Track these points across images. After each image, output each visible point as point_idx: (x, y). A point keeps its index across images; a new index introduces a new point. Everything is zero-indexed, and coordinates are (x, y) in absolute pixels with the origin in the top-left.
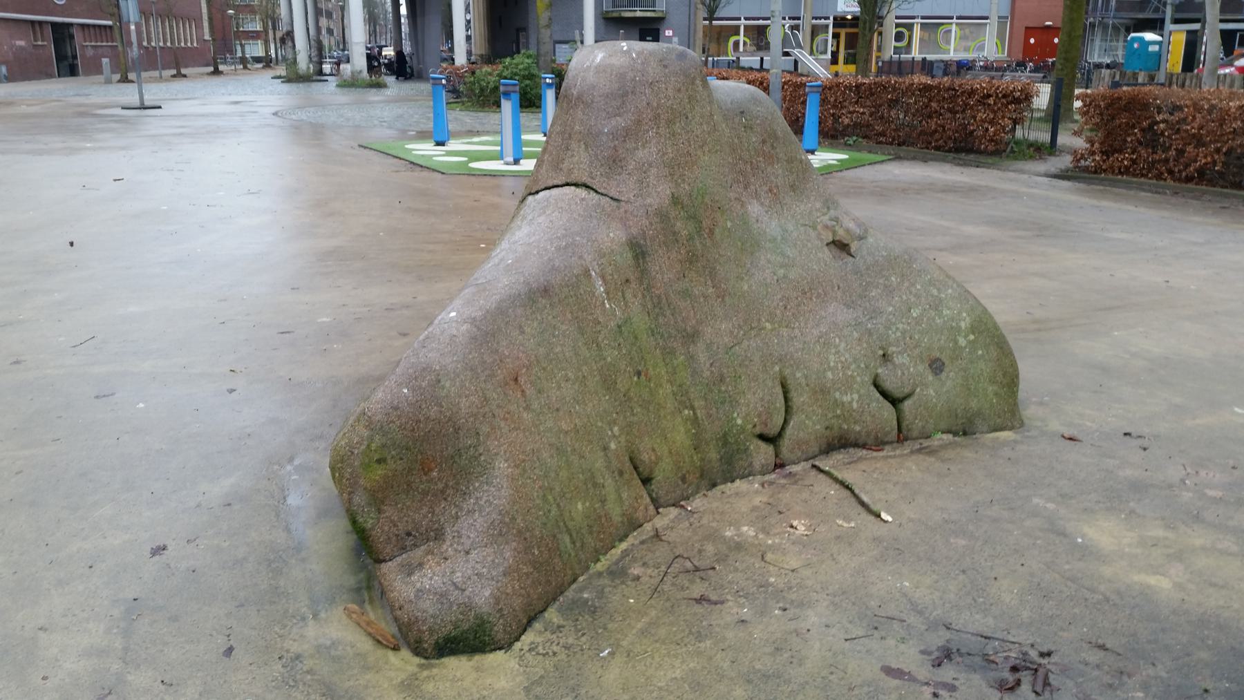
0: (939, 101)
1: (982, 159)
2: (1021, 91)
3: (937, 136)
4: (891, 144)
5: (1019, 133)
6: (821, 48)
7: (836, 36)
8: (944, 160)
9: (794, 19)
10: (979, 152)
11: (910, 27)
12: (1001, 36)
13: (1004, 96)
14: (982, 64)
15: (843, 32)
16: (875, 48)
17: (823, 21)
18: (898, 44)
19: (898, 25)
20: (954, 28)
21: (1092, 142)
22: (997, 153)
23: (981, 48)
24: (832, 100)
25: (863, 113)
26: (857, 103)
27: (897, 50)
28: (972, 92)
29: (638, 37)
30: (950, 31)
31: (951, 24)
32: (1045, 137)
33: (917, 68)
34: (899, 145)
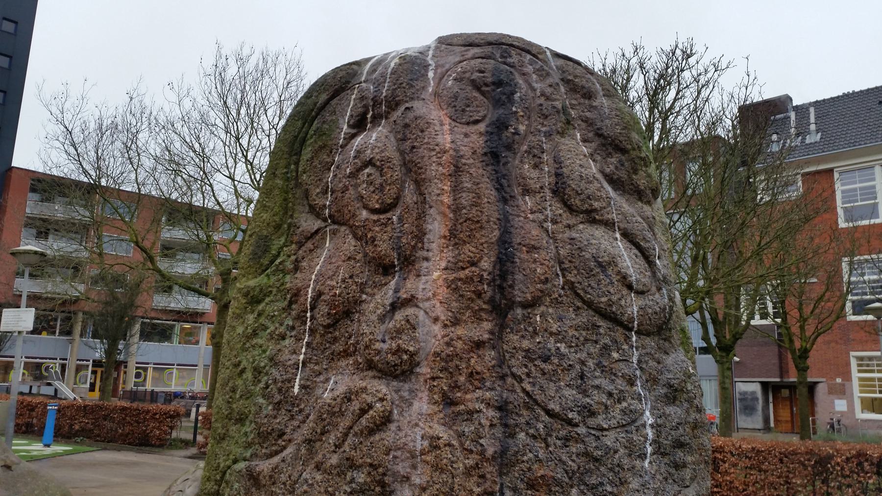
0: (130, 417)
1: (154, 449)
2: (174, 411)
3: (130, 436)
4: (103, 441)
6: (83, 380)
7: (94, 372)
8: (131, 450)
9: (64, 359)
10: (153, 446)
11: (145, 370)
12: (205, 377)
13: (165, 414)
14: (190, 394)
16: (121, 381)
17: (85, 362)
18: (137, 380)
19: (137, 368)
22: (161, 446)
23: (192, 384)
24: (69, 414)
25: (88, 423)
26: (84, 416)
29: (14, 175)
31: (173, 368)
32: (190, 437)
34: (108, 442)
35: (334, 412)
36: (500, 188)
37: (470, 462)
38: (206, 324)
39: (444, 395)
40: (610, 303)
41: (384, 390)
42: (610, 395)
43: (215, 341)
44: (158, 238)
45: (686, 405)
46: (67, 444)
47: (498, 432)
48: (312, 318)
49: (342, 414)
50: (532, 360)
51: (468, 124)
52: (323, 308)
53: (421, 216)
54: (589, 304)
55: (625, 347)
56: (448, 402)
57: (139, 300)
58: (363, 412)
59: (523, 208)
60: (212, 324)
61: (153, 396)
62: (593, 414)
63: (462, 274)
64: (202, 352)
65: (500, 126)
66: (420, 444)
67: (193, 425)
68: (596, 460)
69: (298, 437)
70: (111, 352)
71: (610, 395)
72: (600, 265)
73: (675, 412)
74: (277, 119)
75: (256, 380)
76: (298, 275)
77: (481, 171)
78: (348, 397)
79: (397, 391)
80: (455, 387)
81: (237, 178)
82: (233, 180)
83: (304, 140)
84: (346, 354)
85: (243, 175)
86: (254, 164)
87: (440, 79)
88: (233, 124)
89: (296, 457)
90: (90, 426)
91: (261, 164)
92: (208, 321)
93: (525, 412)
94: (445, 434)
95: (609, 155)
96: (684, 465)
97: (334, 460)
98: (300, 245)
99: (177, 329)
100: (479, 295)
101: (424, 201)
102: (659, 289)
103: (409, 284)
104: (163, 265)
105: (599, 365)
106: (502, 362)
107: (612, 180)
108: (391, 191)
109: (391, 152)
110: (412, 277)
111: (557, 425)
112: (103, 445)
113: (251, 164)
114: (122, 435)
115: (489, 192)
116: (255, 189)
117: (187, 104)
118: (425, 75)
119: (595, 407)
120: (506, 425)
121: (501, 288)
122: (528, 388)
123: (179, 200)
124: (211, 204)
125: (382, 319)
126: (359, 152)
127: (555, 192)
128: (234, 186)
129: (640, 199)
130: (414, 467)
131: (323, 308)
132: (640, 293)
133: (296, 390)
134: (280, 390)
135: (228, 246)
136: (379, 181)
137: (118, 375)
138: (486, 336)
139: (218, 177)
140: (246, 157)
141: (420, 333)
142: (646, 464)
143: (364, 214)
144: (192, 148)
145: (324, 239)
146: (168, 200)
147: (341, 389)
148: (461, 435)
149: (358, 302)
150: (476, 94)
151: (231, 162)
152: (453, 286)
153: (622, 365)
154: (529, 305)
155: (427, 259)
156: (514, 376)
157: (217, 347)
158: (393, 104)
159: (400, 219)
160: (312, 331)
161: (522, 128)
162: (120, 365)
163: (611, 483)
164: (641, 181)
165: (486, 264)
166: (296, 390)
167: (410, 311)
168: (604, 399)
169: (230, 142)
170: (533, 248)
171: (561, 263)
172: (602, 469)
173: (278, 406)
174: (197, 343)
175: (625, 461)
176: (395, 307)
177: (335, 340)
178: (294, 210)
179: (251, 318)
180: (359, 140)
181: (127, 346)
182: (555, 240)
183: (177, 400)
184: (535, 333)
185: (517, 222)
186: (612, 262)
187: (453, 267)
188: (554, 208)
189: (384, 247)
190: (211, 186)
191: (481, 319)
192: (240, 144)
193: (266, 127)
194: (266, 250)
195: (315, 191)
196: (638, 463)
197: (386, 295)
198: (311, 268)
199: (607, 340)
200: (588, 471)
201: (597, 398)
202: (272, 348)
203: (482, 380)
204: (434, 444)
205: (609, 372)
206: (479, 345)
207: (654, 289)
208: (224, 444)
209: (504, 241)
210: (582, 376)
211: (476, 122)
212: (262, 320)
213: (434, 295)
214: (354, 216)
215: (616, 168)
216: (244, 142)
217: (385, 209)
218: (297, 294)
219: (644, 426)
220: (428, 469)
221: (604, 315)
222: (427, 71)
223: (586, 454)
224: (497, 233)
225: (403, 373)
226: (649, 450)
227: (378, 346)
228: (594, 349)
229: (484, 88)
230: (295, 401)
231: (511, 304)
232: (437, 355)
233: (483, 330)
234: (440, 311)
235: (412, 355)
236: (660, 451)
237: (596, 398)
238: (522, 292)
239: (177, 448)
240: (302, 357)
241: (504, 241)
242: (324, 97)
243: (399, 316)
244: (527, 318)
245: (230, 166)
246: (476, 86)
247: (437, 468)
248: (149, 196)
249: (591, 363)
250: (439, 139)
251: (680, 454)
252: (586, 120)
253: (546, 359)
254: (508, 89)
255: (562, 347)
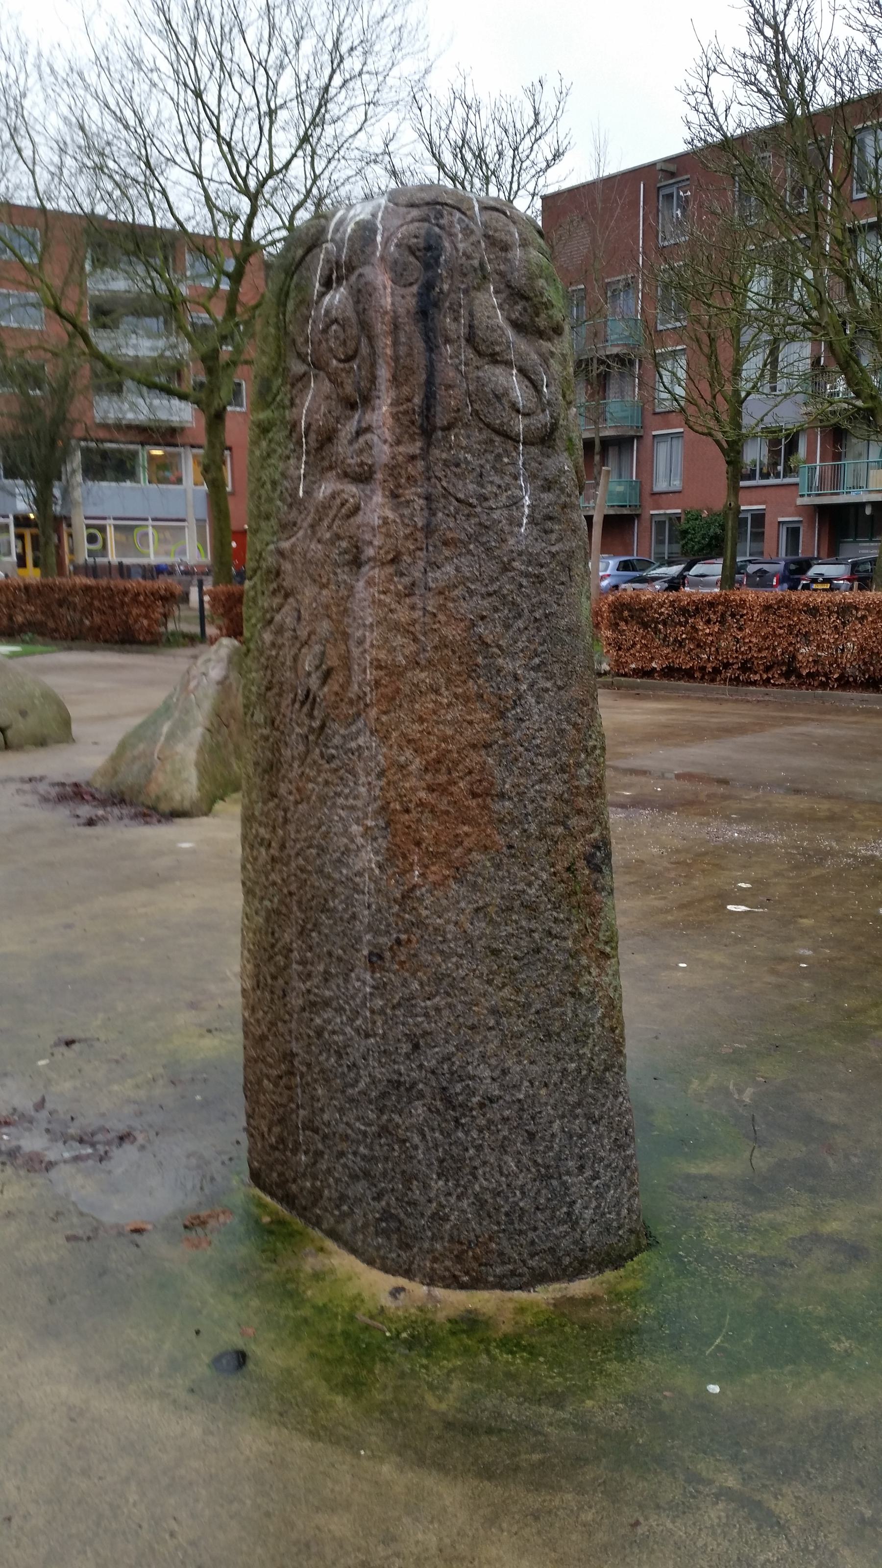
1: (143, 648)
5: (171, 626)
7: (20, 537)
8: (111, 650)
10: (143, 643)
11: (102, 529)
14: (182, 568)
15: (27, 533)
18: (93, 547)
19: (88, 527)
20: (151, 531)
21: (220, 629)
23: (183, 552)
27: (91, 553)
28: (125, 592)
30: (147, 534)
33: (115, 573)
34: (73, 639)
35: (325, 506)
36: (428, 340)
37: (408, 531)
38: (188, 449)
39: (392, 492)
40: (502, 424)
41: (354, 490)
42: (499, 487)
43: (209, 476)
44: (83, 291)
45: (558, 492)
46: (9, 643)
47: (426, 513)
48: (307, 443)
49: (330, 507)
50: (448, 467)
51: (405, 286)
52: (313, 436)
53: (373, 365)
54: (488, 426)
55: (514, 454)
56: (395, 496)
57: (75, 409)
58: (343, 505)
59: (444, 354)
60: (200, 447)
61: (123, 571)
62: (486, 499)
63: (401, 409)
64: (190, 496)
65: (428, 286)
66: (377, 522)
67: (198, 614)
68: (486, 527)
69: (305, 525)
70: (43, 501)
71: (499, 487)
72: (496, 396)
73: (548, 497)
74: (264, 48)
75: (274, 489)
76: (294, 410)
77: (413, 328)
78: (333, 496)
79: (363, 491)
80: (399, 486)
81: (206, 174)
82: (200, 177)
83: (287, 294)
84: (331, 468)
85: (215, 165)
86: (233, 144)
87: (386, 242)
88: (187, 64)
89: (305, 536)
90: (39, 617)
91: (246, 139)
92: (192, 441)
93: (442, 500)
94: (390, 515)
95: (516, 303)
96: (552, 531)
97: (328, 535)
98: (293, 385)
99: (142, 459)
100: (413, 422)
101: (374, 353)
102: (543, 411)
103: (367, 417)
104: (103, 342)
105: (493, 467)
106: (428, 468)
107: (516, 325)
108: (351, 345)
109: (350, 313)
110: (369, 412)
111: (463, 507)
112: (65, 644)
113: (229, 145)
114: (91, 628)
115: (419, 345)
116: (239, 192)
117: (101, 33)
118: (375, 240)
119: (488, 495)
120: (430, 509)
121: (427, 417)
122: (445, 484)
123: (112, 217)
124: (165, 221)
125: (351, 443)
126: (327, 312)
127: (468, 340)
128: (205, 190)
129: (541, 337)
130: (374, 536)
131: (313, 436)
132: (526, 415)
133: (301, 493)
134: (290, 495)
135: (207, 304)
136: (342, 337)
137: (60, 539)
138: (418, 452)
139: (174, 173)
140: (217, 131)
141: (375, 451)
142: (522, 530)
143: (334, 362)
144: (121, 120)
145: (307, 386)
146: (91, 218)
147: (329, 491)
148: (402, 516)
149: (335, 431)
150: (412, 259)
151: (192, 141)
152: (395, 417)
153: (510, 467)
154: (447, 428)
155: (379, 398)
156: (436, 477)
157: (216, 486)
158: (351, 268)
159: (359, 367)
160: (308, 453)
161: (446, 287)
162: (61, 522)
163: (495, 541)
164: (542, 322)
165: (417, 400)
166: (301, 493)
167: (368, 436)
168: (495, 489)
169: (186, 102)
170: (449, 387)
171: (470, 396)
172: (491, 533)
173: (290, 506)
174: (179, 481)
175: (507, 528)
176: (359, 433)
177: (323, 458)
178: (285, 355)
179: (264, 444)
180: (327, 298)
181: (66, 492)
182: (467, 378)
183: (161, 577)
184: (451, 448)
185: (439, 366)
186: (506, 393)
187: (395, 403)
188: (467, 353)
189: (349, 389)
190: (164, 193)
191: (414, 440)
192: (204, 103)
193: (247, 65)
194: (269, 389)
195: (300, 340)
196: (516, 529)
197: (351, 427)
198: (303, 405)
199: (501, 450)
200: (481, 535)
201: (490, 489)
202: (281, 466)
203: (416, 481)
204: (385, 521)
205: (501, 472)
206: (413, 458)
207: (539, 411)
208: (258, 535)
209: (430, 382)
210: (481, 475)
211: (411, 284)
212: (273, 445)
213: (384, 424)
214: (328, 364)
215: (521, 314)
216: (211, 98)
217: (349, 359)
218: (295, 425)
219: (523, 506)
220: (382, 537)
221: (498, 432)
222: (375, 235)
223: (480, 524)
224: (424, 377)
225: (366, 479)
226: (525, 521)
227: (349, 461)
228: (490, 457)
229: (418, 253)
230: (301, 502)
231: (434, 429)
232: (386, 465)
233: (415, 448)
234: (387, 435)
235: (370, 467)
236: (532, 521)
237: (489, 489)
238: (441, 420)
239: (178, 645)
240: (302, 471)
241: (430, 382)
242: (300, 252)
243: (361, 440)
244: (446, 438)
245: (190, 147)
246: (412, 251)
247: (388, 535)
248: (59, 214)
249: (488, 467)
250: (383, 302)
251: (549, 525)
252: (502, 274)
253: (457, 465)
254: (436, 253)
255: (469, 456)
